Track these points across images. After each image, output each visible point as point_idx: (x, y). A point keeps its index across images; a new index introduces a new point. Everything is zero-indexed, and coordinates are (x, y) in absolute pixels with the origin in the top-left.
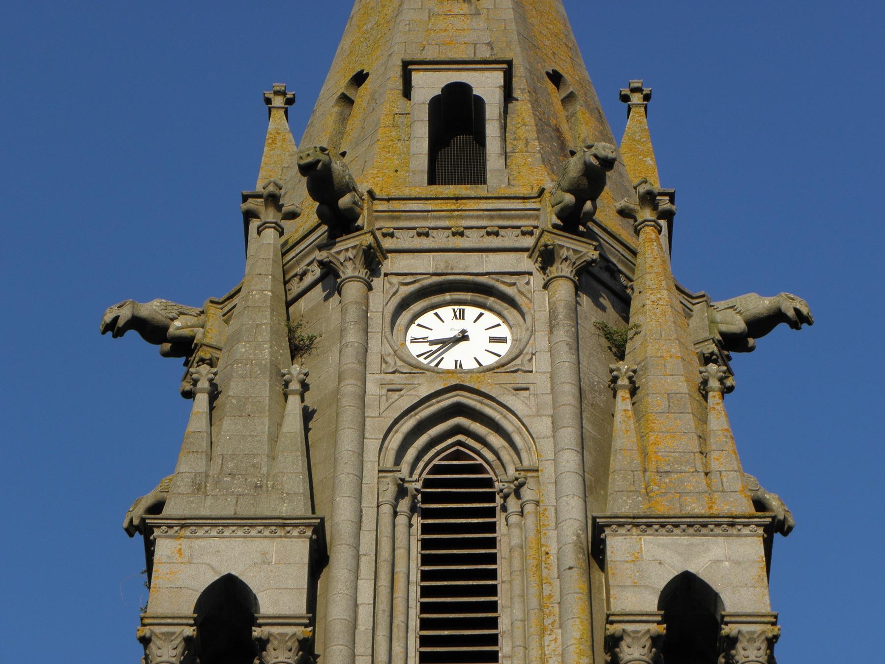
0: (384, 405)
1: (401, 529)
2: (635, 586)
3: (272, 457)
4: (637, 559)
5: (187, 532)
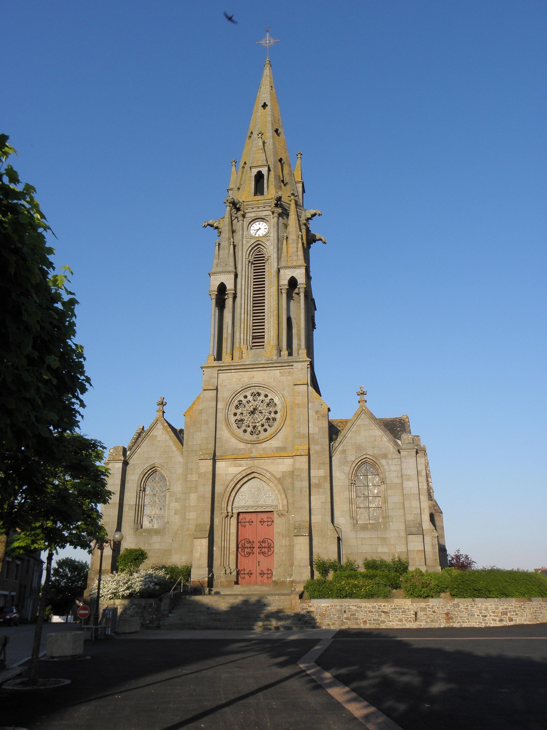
0: (246, 245)
1: (250, 269)
2: (284, 279)
3: (228, 258)
4: (285, 274)
5: (215, 275)
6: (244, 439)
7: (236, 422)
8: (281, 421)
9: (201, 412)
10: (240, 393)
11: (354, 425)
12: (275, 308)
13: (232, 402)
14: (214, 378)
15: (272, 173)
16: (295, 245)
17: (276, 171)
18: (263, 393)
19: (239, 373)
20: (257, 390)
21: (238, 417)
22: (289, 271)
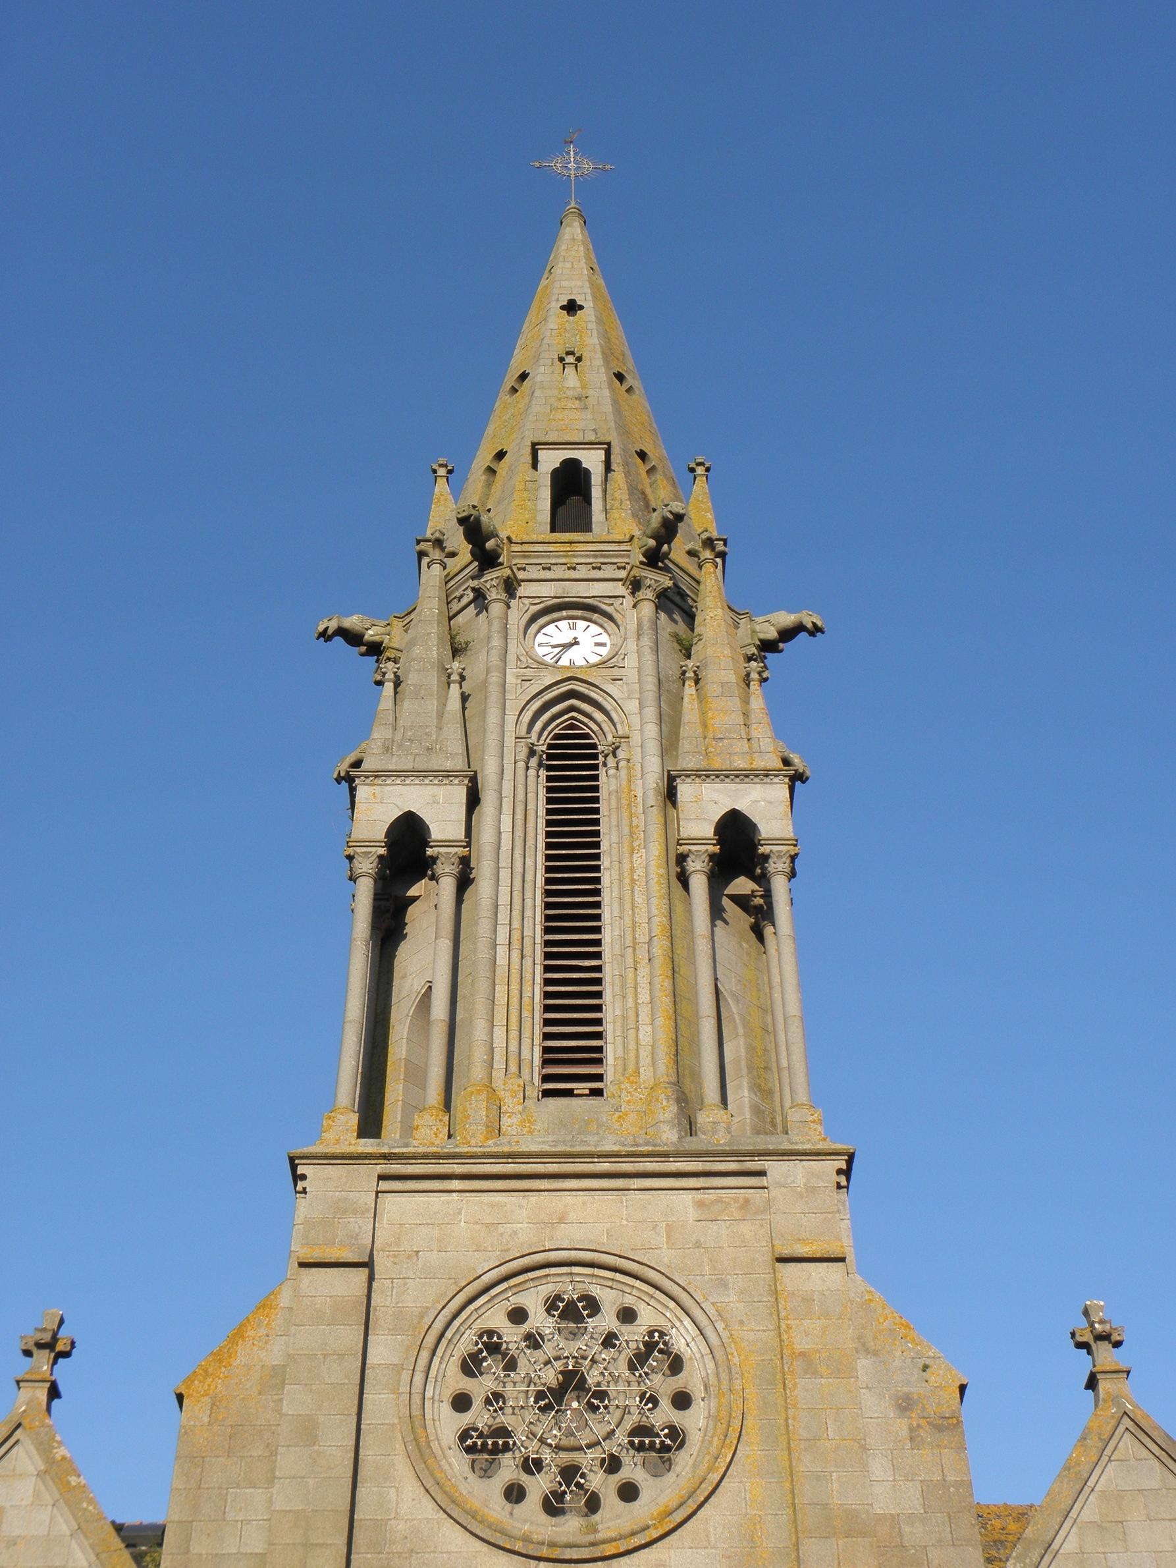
2: (698, 819)
6: (515, 1532)
7: (469, 1442)
8: (716, 1441)
9: (276, 1378)
10: (494, 1292)
11: (1087, 1490)
12: (656, 930)
13: (449, 1334)
14: (355, 1212)
15: (618, 476)
16: (736, 703)
17: (630, 475)
18: (610, 1300)
19: (485, 1197)
20: (570, 1286)
21: (479, 1417)
22: (718, 791)
